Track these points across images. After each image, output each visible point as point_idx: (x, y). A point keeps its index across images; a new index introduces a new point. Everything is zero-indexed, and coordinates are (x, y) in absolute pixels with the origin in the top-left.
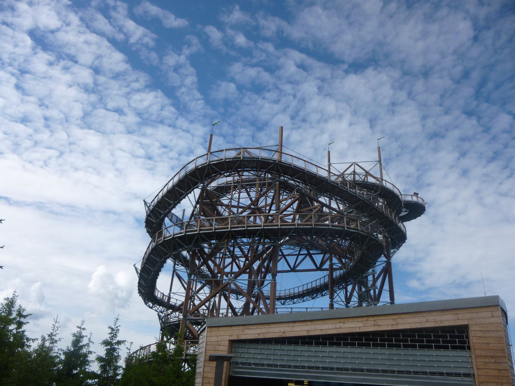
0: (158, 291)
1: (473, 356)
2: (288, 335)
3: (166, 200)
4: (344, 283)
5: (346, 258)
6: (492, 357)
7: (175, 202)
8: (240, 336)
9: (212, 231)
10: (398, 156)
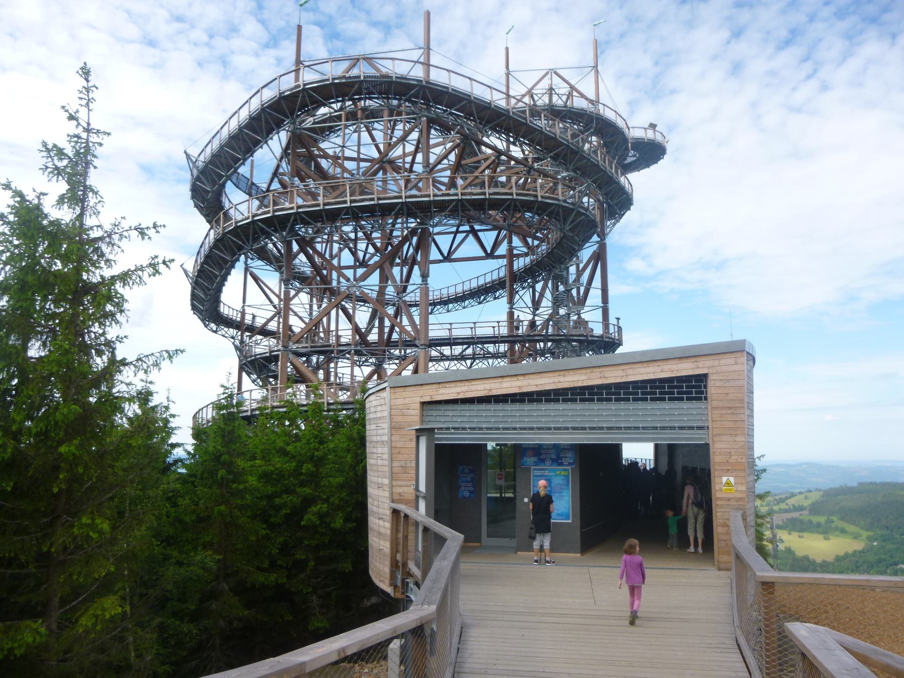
0: (224, 304)
1: (709, 408)
3: (227, 152)
4: (531, 278)
5: (535, 238)
6: (730, 408)
7: (244, 156)
8: (434, 396)
10: (622, 36)
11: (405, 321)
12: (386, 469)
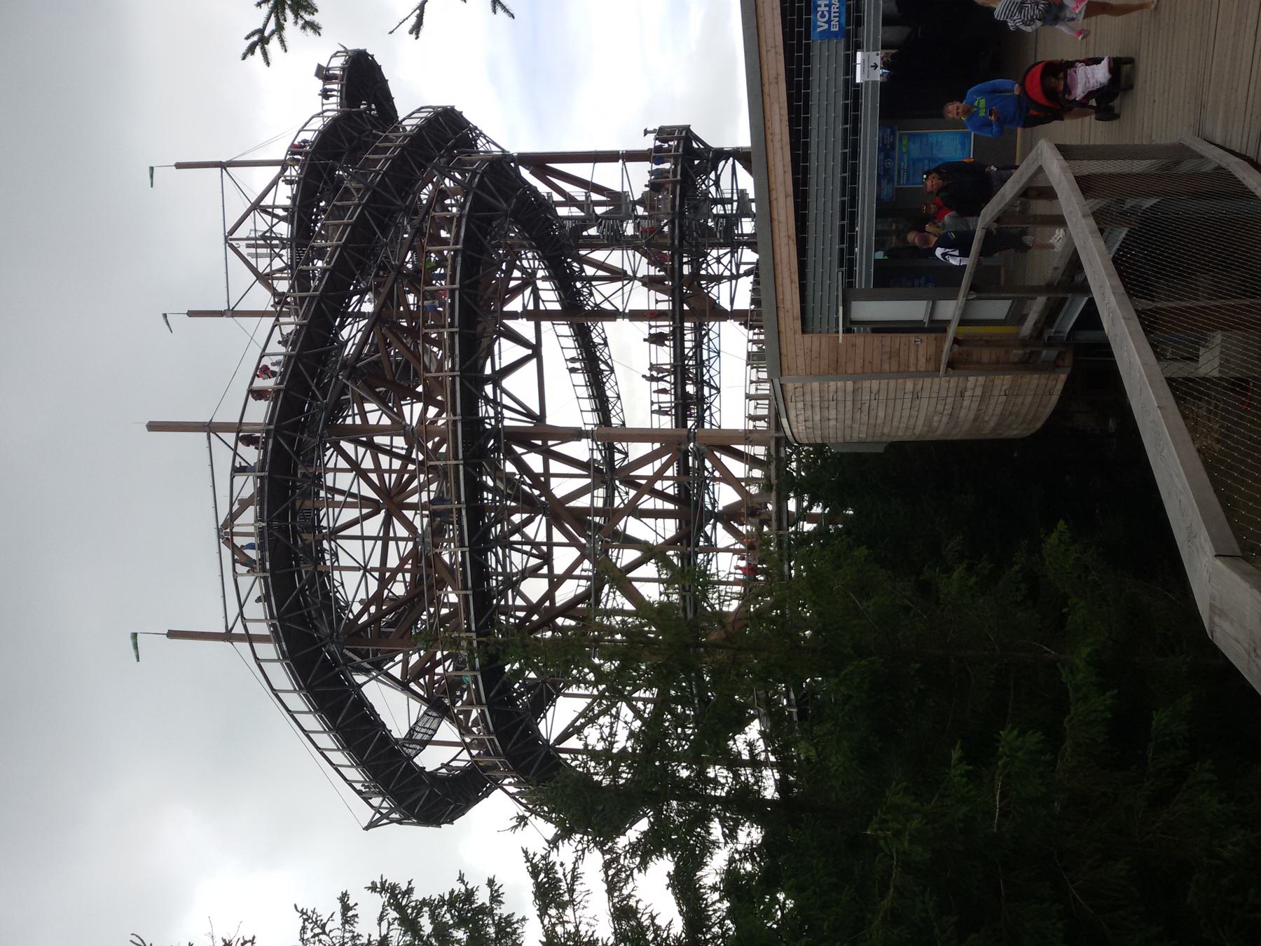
2: (792, 231)
9: (471, 598)
11: (647, 470)
12: (892, 383)
